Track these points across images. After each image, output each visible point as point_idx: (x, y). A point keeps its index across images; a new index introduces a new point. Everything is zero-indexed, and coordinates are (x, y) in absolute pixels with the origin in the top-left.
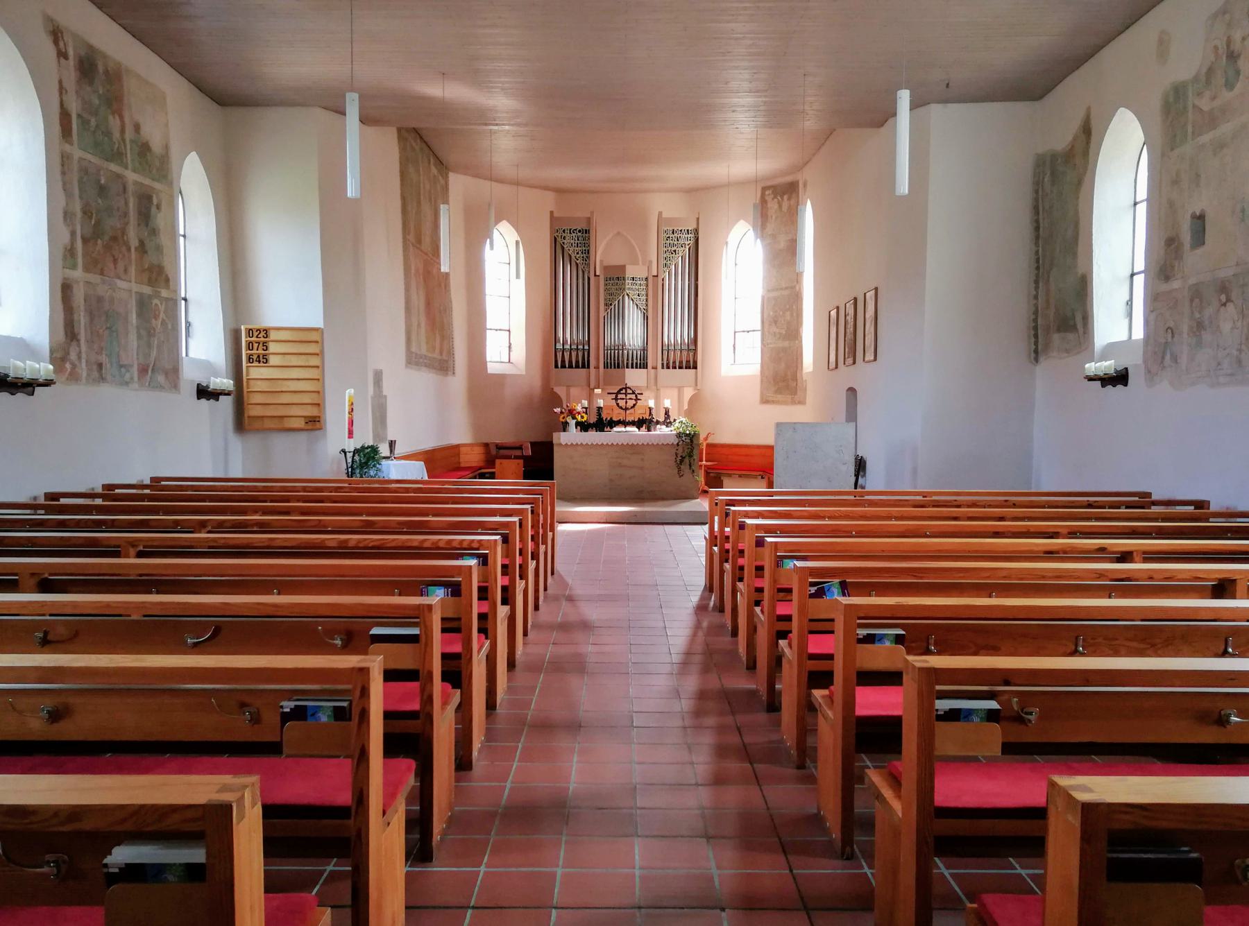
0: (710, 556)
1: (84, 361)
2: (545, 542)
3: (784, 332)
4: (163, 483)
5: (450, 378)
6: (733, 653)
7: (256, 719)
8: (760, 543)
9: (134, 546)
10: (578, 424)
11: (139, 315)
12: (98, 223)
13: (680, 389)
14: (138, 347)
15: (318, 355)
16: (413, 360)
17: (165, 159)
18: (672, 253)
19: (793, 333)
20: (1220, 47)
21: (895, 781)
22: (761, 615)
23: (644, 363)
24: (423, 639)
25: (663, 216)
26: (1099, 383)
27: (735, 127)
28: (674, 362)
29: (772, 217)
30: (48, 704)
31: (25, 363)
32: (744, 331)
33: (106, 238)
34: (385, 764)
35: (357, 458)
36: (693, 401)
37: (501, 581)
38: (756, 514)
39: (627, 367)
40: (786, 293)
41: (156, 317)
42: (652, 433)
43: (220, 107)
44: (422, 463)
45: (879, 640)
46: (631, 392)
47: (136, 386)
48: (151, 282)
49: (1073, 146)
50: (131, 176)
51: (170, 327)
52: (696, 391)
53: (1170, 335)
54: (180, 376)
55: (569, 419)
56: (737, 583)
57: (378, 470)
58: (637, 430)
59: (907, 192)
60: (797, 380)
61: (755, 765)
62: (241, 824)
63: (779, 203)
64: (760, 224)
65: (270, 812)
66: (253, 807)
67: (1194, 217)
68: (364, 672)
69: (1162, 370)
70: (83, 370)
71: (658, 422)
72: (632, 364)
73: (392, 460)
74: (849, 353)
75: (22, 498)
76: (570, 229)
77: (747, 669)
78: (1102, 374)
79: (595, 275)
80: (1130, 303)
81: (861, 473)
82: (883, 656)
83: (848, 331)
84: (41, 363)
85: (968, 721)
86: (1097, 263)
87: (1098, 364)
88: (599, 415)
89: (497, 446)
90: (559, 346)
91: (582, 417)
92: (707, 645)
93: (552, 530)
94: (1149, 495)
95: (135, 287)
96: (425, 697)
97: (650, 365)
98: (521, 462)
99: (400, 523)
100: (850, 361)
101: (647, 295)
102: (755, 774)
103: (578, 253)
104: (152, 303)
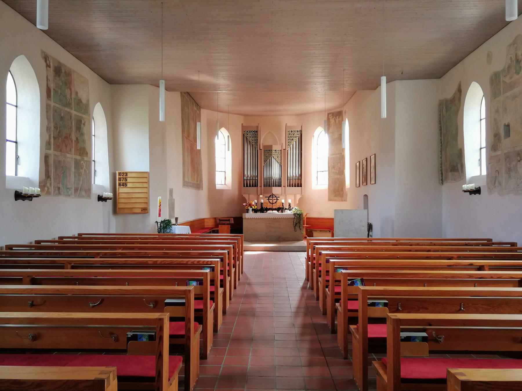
0: (308, 266)
1: (52, 186)
2: (239, 260)
3: (338, 172)
4: (83, 236)
5: (201, 191)
6: (318, 307)
7: (117, 340)
8: (328, 261)
9: (70, 264)
10: (253, 210)
11: (75, 168)
12: (60, 132)
13: (295, 195)
14: (75, 180)
15: (147, 183)
16: (186, 184)
17: (87, 106)
18: (291, 140)
19: (341, 172)
20: (513, 57)
21: (384, 366)
22: (328, 292)
23: (280, 185)
24: (187, 304)
25: (288, 125)
26: (468, 193)
27: (316, 90)
28: (292, 184)
29: (332, 125)
30: (31, 333)
31: (29, 188)
32: (321, 171)
33: (63, 137)
34: (170, 358)
35: (162, 225)
36: (300, 200)
37: (220, 277)
38: (326, 249)
39: (273, 186)
40: (338, 156)
41: (82, 168)
42: (284, 213)
43: (110, 85)
44: (189, 227)
45: (377, 305)
46: (275, 196)
47: (73, 196)
48: (81, 154)
49: (454, 97)
50: (74, 112)
51: (87, 172)
52: (301, 196)
53: (497, 173)
54: (91, 193)
55: (249, 208)
56: (319, 278)
57: (171, 230)
58: (277, 212)
59: (386, 117)
60: (343, 191)
61: (326, 357)
62: (108, 388)
63: (335, 119)
64: (327, 128)
65: (121, 379)
66: (114, 380)
67: (505, 125)
68: (161, 320)
69: (495, 188)
70: (52, 190)
71: (286, 209)
72: (275, 185)
73: (177, 225)
74: (364, 180)
75: (26, 243)
76: (250, 131)
77: (323, 314)
78: (469, 189)
79: (260, 149)
80: (480, 160)
81: (371, 230)
82: (379, 311)
83: (364, 171)
84: (36, 188)
85: (414, 341)
86: (466, 144)
87: (468, 185)
88: (262, 206)
89: (219, 219)
90: (245, 178)
91: (255, 207)
92: (306, 304)
93: (242, 254)
94: (491, 240)
95: (74, 157)
96: (187, 329)
97: (282, 185)
98: (229, 226)
99: (178, 253)
100: (365, 184)
101: (281, 157)
102: (327, 362)
103: (253, 140)
104: (80, 163)
